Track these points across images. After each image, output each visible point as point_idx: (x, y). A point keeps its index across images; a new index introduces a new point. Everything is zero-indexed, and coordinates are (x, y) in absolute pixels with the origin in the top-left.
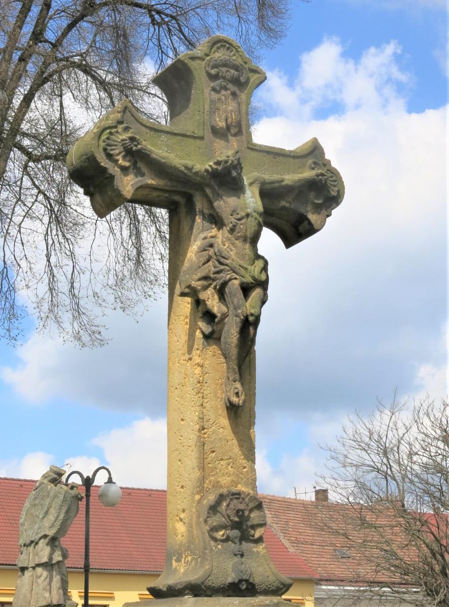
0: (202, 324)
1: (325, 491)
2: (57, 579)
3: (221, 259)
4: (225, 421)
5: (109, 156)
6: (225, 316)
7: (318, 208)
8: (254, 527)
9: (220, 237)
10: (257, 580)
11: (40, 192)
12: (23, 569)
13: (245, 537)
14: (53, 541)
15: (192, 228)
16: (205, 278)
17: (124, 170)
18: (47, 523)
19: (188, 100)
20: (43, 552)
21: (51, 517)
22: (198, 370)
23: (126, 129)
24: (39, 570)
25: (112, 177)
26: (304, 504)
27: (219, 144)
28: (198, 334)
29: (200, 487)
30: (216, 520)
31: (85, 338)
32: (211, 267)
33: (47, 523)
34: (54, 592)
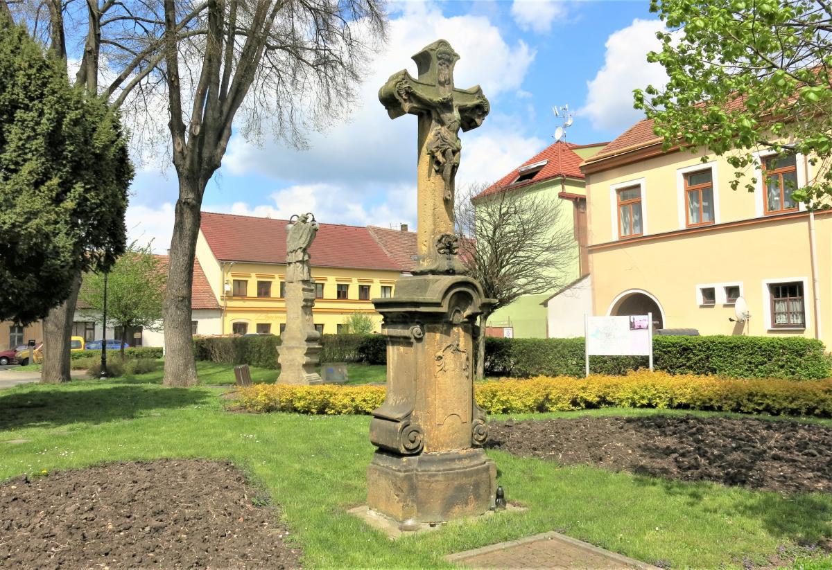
0: (435, 166)
1: (406, 226)
2: (306, 268)
3: (443, 139)
4: (443, 206)
5: (400, 95)
6: (445, 163)
7: (479, 117)
8: (455, 248)
9: (444, 130)
10: (456, 269)
11: (273, 66)
12: (290, 263)
13: (451, 252)
14: (304, 251)
15: (430, 125)
16: (437, 147)
17: (405, 100)
18: (301, 242)
19: (428, 68)
20: (300, 256)
21: (303, 239)
22: (433, 185)
23: (406, 82)
24: (298, 264)
25: (400, 104)
26: (397, 233)
27: (441, 89)
28: (433, 170)
29: (434, 232)
30: (440, 245)
31: (299, 146)
32: (439, 143)
33: (301, 242)
34: (305, 274)
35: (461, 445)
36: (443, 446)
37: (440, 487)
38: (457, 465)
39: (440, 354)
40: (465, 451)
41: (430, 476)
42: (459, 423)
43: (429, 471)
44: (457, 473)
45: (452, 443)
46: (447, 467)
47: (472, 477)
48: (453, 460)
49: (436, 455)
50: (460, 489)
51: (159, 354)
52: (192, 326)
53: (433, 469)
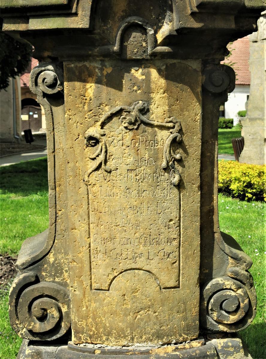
35: (158, 336)
36: (109, 334)
39: (95, 131)
40: (170, 349)
42: (152, 288)
45: (134, 331)
51: (229, 125)
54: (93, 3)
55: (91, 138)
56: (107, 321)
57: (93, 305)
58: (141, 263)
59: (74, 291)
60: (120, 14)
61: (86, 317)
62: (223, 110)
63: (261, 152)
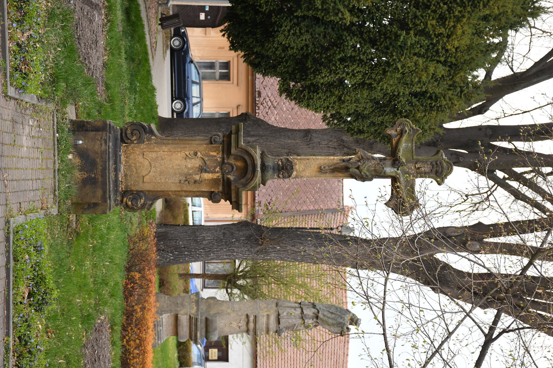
36: (127, 157)
37: (97, 147)
38: (112, 166)
41: (105, 141)
42: (144, 173)
43: (109, 140)
44: (106, 162)
46: (111, 155)
47: (102, 176)
48: (116, 163)
49: (120, 151)
50: (93, 164)
52: (231, 334)
53: (111, 144)
54: (549, 156)
55: (197, 153)
56: (132, 156)
57: (138, 152)
58: (153, 169)
59: (142, 146)
60: (236, 164)
61: (133, 149)
62: (210, 358)
63: (163, 311)
